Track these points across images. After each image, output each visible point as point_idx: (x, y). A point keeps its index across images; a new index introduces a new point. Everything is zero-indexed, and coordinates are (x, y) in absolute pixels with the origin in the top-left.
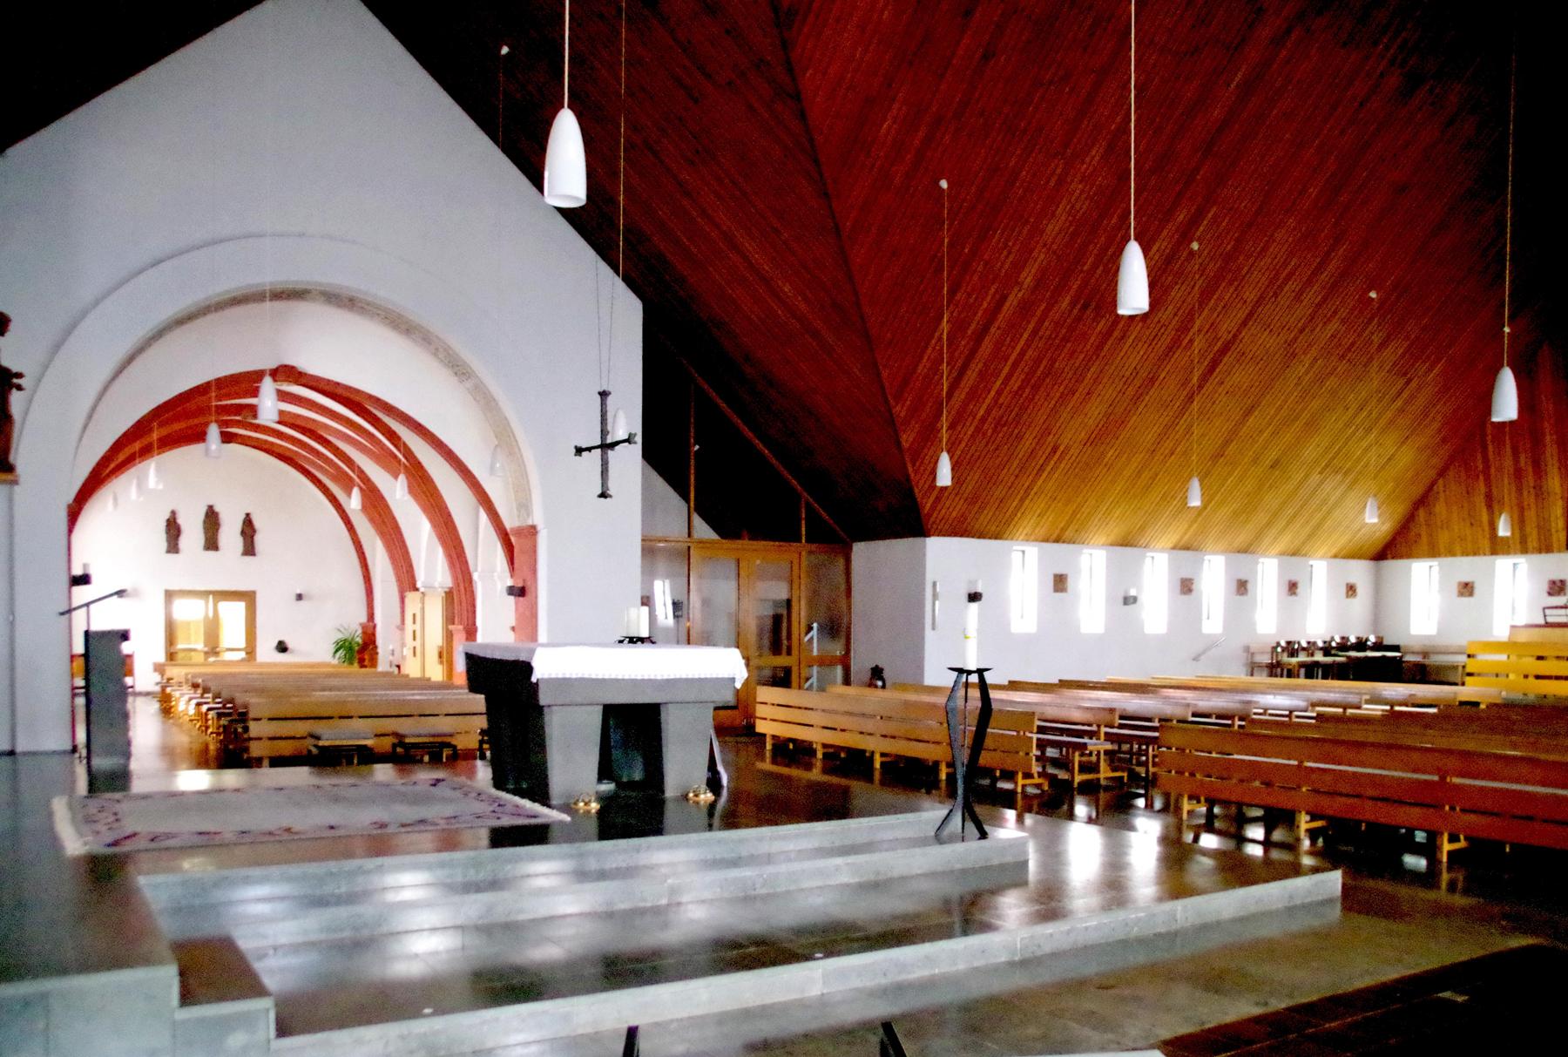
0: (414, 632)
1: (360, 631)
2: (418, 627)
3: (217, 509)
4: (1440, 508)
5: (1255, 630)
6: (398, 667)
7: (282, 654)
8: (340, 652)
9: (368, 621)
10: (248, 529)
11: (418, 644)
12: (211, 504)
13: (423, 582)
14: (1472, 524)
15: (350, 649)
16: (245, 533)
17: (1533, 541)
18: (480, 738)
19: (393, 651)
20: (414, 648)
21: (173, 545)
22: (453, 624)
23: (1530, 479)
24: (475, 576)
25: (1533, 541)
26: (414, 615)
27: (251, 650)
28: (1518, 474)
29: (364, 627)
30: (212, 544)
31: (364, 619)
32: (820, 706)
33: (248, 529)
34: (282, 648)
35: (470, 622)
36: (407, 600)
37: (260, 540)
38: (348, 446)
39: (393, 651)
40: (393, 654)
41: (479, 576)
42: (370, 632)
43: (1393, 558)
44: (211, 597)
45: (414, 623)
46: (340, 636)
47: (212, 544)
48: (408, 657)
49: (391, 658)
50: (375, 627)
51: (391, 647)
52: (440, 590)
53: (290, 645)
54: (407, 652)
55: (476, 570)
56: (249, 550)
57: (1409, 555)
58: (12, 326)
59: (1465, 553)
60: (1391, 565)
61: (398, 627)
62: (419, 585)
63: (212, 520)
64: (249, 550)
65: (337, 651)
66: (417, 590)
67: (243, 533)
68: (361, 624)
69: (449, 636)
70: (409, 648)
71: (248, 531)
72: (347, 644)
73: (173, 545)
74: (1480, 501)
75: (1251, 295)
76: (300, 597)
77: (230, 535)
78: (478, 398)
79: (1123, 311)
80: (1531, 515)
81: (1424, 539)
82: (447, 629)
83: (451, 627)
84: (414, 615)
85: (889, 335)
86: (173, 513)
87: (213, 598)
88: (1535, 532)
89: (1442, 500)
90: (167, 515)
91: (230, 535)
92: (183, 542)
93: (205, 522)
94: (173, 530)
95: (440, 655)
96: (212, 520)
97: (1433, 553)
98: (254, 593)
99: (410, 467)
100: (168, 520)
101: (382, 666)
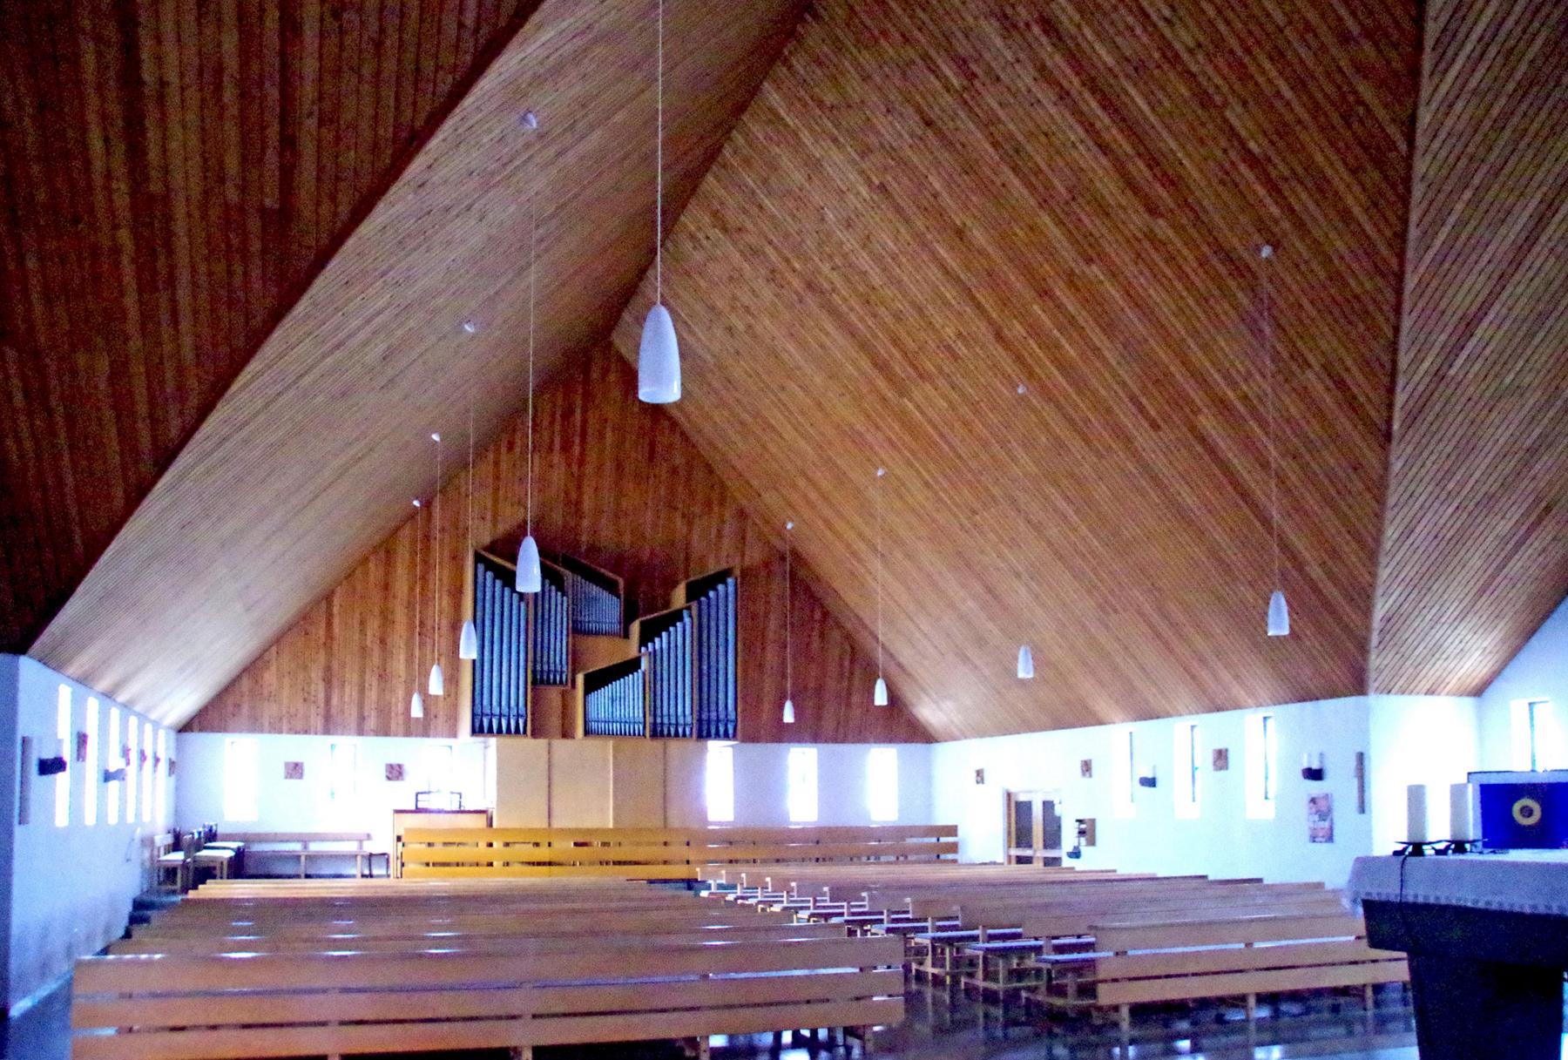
4: (270, 677)
14: (305, 700)
17: (371, 723)
18: (1464, 780)
23: (376, 658)
25: (371, 723)
28: (364, 651)
32: (202, 1019)
38: (240, 378)
43: (201, 730)
57: (223, 729)
58: (1361, 854)
59: (294, 731)
60: (197, 739)
74: (316, 673)
75: (863, 570)
79: (646, 394)
80: (372, 695)
81: (245, 709)
85: (485, 140)
88: (373, 713)
89: (273, 668)
97: (255, 726)
99: (217, 955)
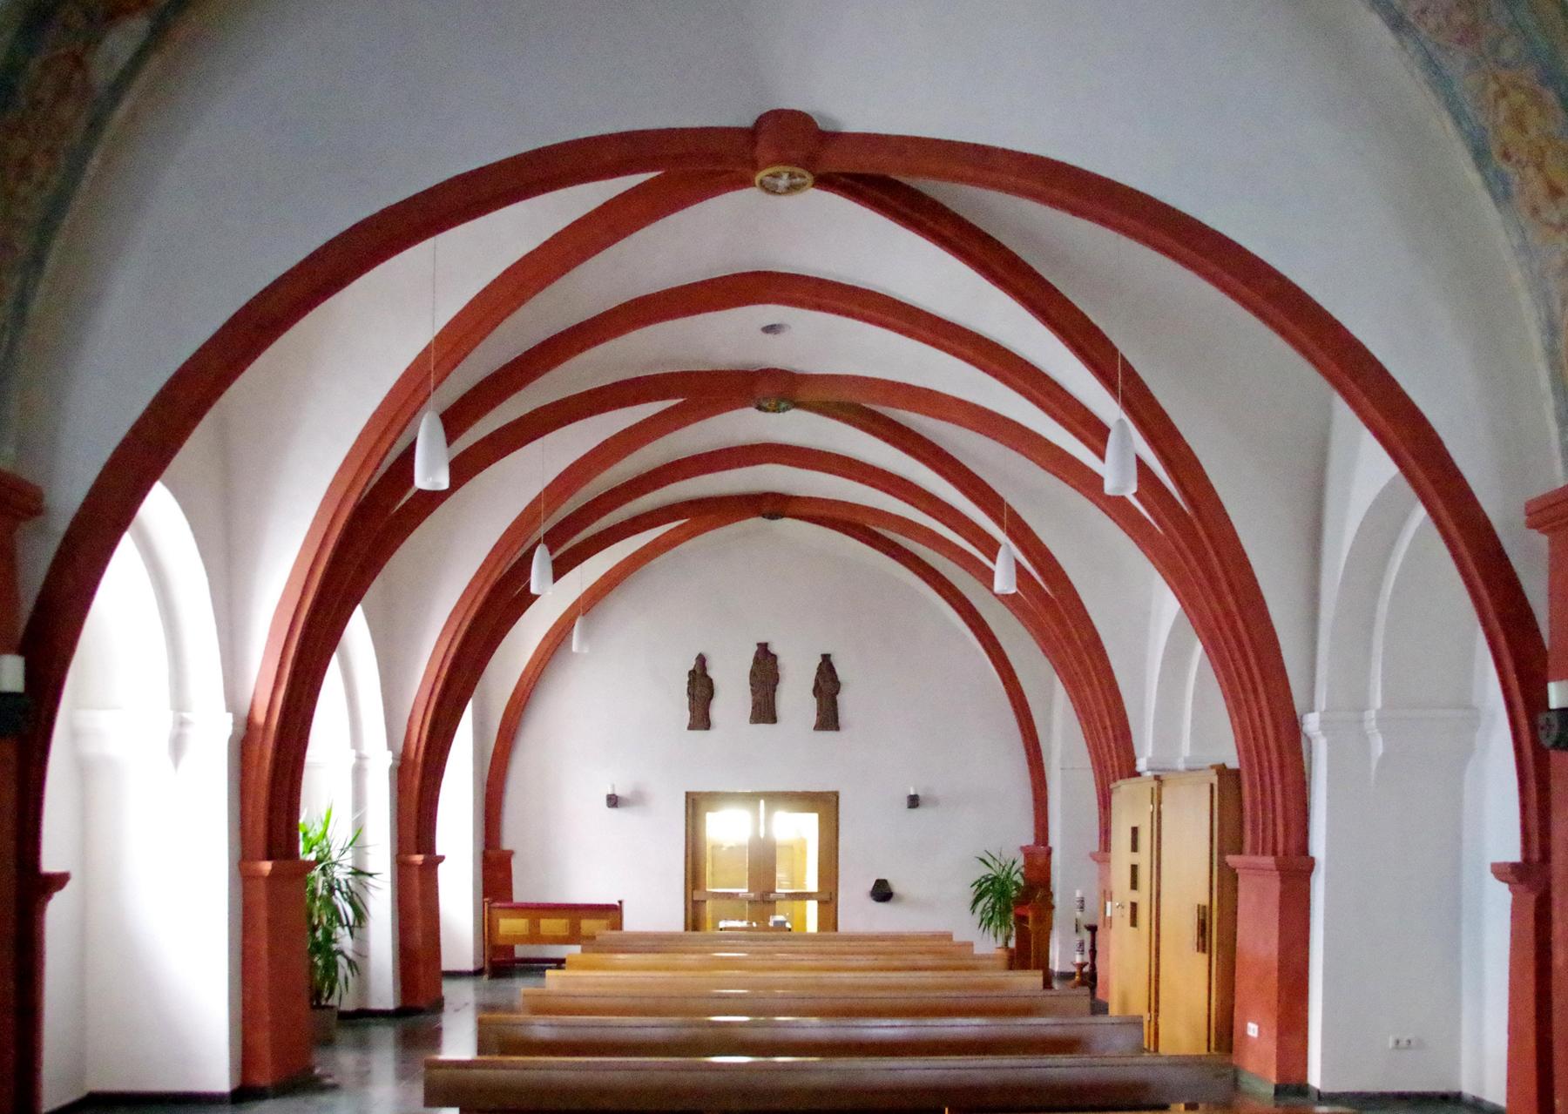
0: (1134, 868)
1: (1021, 862)
2: (1143, 859)
3: (774, 648)
5: (708, 811)
6: (1093, 929)
7: (881, 906)
8: (985, 900)
9: (1037, 843)
10: (827, 683)
11: (1143, 897)
12: (763, 640)
13: (1149, 761)
15: (1002, 894)
16: (821, 691)
19: (1082, 901)
20: (1134, 906)
21: (701, 718)
22: (1240, 852)
24: (1311, 723)
26: (1135, 831)
27: (828, 902)
29: (1028, 853)
30: (765, 711)
31: (1029, 840)
33: (827, 683)
34: (882, 892)
35: (1292, 844)
36: (1116, 800)
37: (847, 702)
39: (1082, 901)
40: (1082, 908)
41: (1325, 724)
42: (1040, 861)
44: (762, 802)
45: (1135, 848)
46: (985, 871)
47: (765, 711)
48: (1116, 922)
49: (1079, 914)
50: (1049, 852)
51: (1078, 894)
52: (1149, 774)
53: (896, 887)
54: (1116, 911)
55: (1312, 710)
56: (828, 719)
61: (1093, 856)
62: (1141, 765)
63: (765, 669)
64: (828, 719)
65: (976, 901)
66: (1138, 774)
67: (817, 691)
68: (1023, 848)
69: (1226, 881)
70: (1122, 906)
71: (827, 687)
72: (997, 885)
73: (701, 718)
76: (914, 802)
77: (796, 695)
78: (1133, 534)
82: (1223, 865)
83: (1231, 859)
84: (1135, 831)
86: (701, 660)
87: (766, 803)
90: (691, 664)
91: (796, 695)
92: (717, 710)
93: (753, 674)
94: (701, 687)
95: (1203, 928)
96: (765, 669)
98: (836, 794)
100: (692, 673)
101: (1114, 1010)
